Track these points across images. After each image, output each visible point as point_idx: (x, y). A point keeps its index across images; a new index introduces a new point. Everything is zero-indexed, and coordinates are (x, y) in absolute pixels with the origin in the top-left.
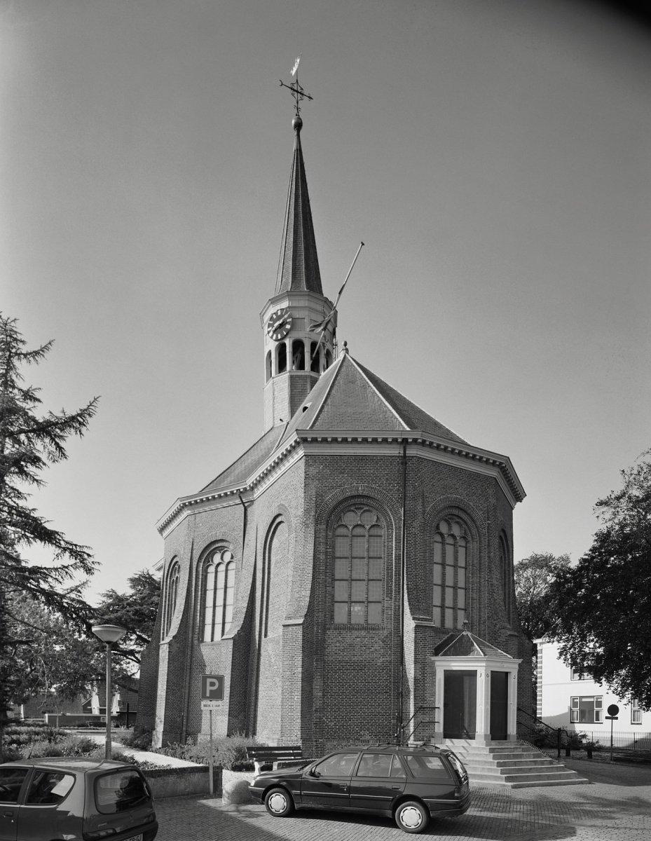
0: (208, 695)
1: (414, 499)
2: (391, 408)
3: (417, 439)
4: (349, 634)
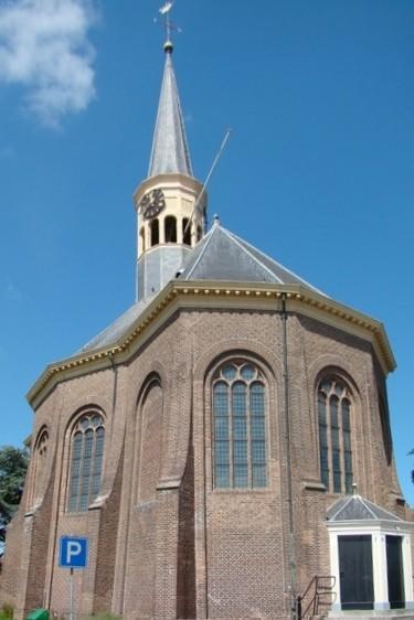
0: (69, 561)
1: (297, 354)
2: (265, 267)
3: (295, 295)
4: (233, 499)
